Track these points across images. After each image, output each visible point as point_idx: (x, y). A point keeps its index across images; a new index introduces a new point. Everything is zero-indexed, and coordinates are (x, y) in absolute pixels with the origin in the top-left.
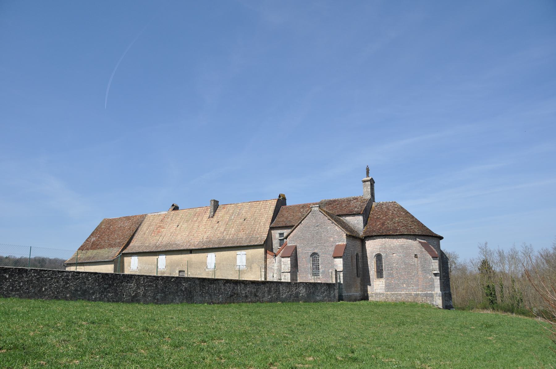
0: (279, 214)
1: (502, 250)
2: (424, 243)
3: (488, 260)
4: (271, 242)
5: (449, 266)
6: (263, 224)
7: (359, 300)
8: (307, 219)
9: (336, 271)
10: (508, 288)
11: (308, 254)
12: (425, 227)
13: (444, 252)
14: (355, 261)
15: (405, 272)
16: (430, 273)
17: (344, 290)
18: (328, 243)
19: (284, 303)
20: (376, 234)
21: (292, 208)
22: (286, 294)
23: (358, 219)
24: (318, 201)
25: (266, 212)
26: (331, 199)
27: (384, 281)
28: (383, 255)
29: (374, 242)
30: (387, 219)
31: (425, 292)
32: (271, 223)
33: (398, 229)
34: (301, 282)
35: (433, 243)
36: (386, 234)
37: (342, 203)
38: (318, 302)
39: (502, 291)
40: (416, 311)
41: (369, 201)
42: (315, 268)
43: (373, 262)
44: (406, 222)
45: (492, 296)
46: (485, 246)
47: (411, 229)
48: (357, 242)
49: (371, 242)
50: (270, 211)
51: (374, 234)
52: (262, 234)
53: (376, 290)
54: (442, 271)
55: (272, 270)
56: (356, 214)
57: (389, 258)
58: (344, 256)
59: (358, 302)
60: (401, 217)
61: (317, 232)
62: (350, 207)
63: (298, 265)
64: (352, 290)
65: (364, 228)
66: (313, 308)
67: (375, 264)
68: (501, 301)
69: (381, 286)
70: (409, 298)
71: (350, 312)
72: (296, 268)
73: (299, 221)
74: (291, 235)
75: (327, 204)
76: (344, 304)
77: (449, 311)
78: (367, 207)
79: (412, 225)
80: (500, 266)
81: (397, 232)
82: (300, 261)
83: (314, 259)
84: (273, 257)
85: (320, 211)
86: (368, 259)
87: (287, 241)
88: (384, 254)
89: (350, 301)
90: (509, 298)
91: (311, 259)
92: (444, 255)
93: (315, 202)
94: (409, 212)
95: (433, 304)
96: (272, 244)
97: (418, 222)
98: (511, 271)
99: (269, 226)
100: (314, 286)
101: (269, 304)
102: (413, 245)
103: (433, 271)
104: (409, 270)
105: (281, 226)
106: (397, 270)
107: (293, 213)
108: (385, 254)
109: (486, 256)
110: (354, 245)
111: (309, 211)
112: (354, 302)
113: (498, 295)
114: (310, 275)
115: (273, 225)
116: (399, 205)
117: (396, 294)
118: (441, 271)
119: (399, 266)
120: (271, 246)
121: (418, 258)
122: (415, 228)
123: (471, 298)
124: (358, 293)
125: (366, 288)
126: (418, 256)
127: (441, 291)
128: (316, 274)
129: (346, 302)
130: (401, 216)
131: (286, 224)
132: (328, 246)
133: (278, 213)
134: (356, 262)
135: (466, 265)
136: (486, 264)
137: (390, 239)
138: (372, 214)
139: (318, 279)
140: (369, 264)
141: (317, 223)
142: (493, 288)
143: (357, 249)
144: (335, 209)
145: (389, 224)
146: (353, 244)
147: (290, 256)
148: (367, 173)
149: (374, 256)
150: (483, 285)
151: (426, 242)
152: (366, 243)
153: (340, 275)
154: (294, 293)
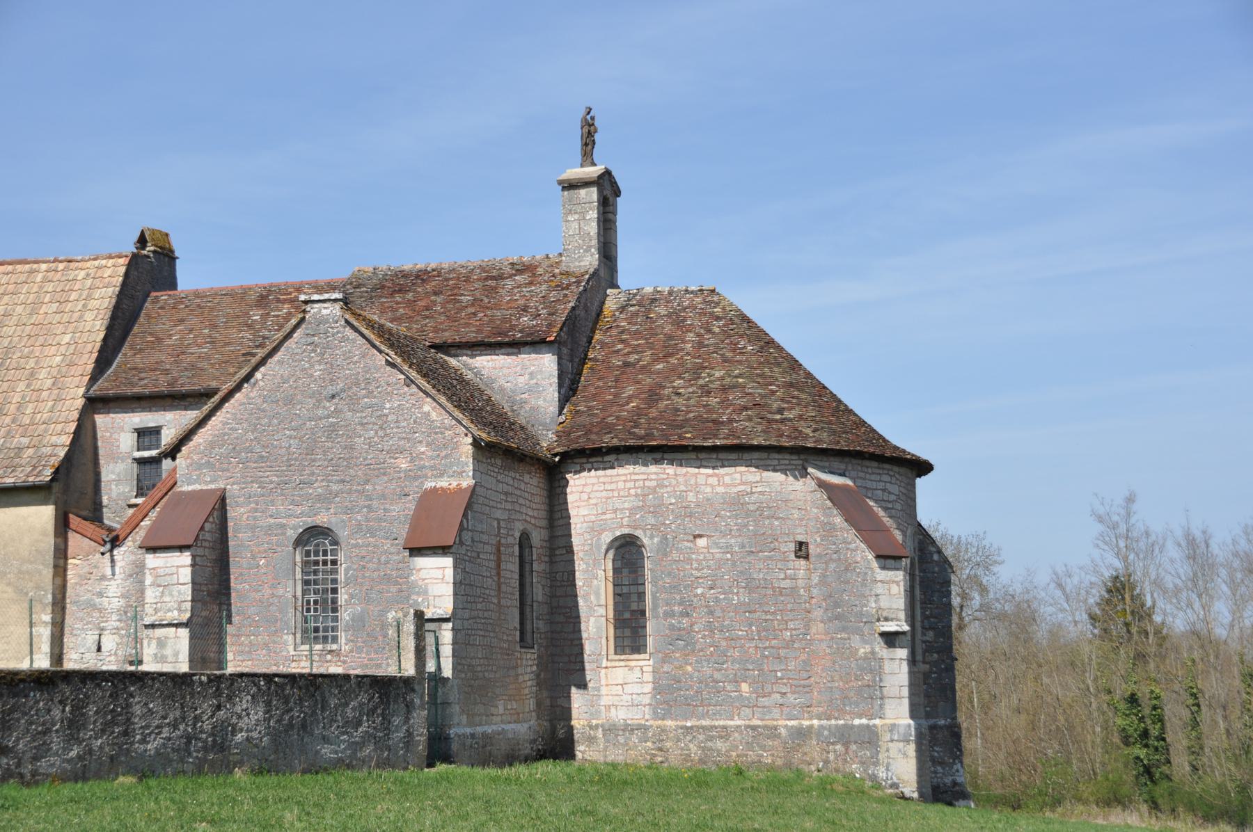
0: (136, 329)
1: (1204, 532)
2: (844, 488)
3: (1138, 575)
4: (91, 476)
5: (956, 601)
6: (49, 382)
7: (527, 760)
8: (281, 362)
9: (419, 615)
10: (1224, 708)
11: (284, 534)
12: (850, 412)
13: (936, 535)
14: (515, 567)
15: (751, 625)
16: (866, 630)
17: (456, 709)
18: (386, 478)
19: (152, 782)
20: (615, 442)
21: (202, 302)
22: (166, 732)
23: (533, 368)
24: (342, 273)
25: (66, 318)
27: (650, 669)
28: (646, 541)
30: (671, 372)
31: (842, 722)
32: (94, 378)
33: (725, 418)
34: (246, 670)
35: (884, 490)
37: (456, 287)
38: (326, 770)
39: (1195, 724)
40: (795, 810)
41: (588, 281)
42: (316, 602)
43: (601, 573)
44: (760, 385)
45: (1146, 746)
46: (1123, 512)
47: (783, 421)
48: (527, 478)
49: (594, 480)
50: (89, 316)
51: (608, 440)
52: (46, 431)
53: (608, 708)
54: (922, 622)
55: (96, 614)
56: (525, 344)
57: (675, 555)
58: (461, 543)
59: (521, 770)
60: (740, 362)
61: (332, 425)
62: (497, 307)
63: (228, 588)
64: (493, 710)
65: (560, 414)
66: (298, 803)
68: (1188, 768)
69: (637, 689)
70: (763, 748)
71: (483, 818)
72: (221, 604)
73: (240, 368)
74: (199, 439)
75: (383, 287)
76: (455, 777)
77: (948, 809)
79: (788, 402)
80: (1190, 605)
81: (716, 436)
83: (313, 558)
84: (102, 549)
85: (347, 322)
86: (577, 563)
87: (174, 470)
88: (652, 537)
89: (484, 763)
90: (1229, 754)
91: (298, 559)
92: (933, 549)
93: (323, 276)
95: (874, 778)
96: (97, 475)
97: (819, 391)
98: (1241, 629)
99: (81, 391)
100: (308, 690)
101: (67, 790)
102: (791, 497)
103: (878, 620)
104: (769, 617)
105: (147, 391)
106: (711, 613)
107: (214, 326)
108: (656, 540)
109: (1125, 559)
110: (511, 489)
111: (294, 321)
112: (501, 765)
113: (1178, 740)
114: (291, 637)
115: (104, 386)
116: (731, 304)
117: (703, 728)
118: (918, 625)
120: (90, 490)
121: (812, 559)
123: (1050, 752)
124: (526, 726)
125: (559, 702)
126: (812, 549)
127: (912, 717)
128: (321, 634)
129: (465, 769)
130: (738, 358)
131: (175, 379)
132: (383, 497)
133: (131, 329)
134: (517, 576)
135: (1035, 598)
136: (1127, 597)
137: (681, 466)
138: (603, 345)
139: (329, 657)
140: (579, 583)
141: (332, 380)
142: (1155, 708)
143: (524, 510)
144: (427, 313)
145: (678, 394)
146: (506, 488)
147: (190, 542)
148: (586, 144)
149: (604, 547)
150: (1109, 692)
151: (849, 482)
152: (568, 482)
153: (437, 638)
154: (207, 726)
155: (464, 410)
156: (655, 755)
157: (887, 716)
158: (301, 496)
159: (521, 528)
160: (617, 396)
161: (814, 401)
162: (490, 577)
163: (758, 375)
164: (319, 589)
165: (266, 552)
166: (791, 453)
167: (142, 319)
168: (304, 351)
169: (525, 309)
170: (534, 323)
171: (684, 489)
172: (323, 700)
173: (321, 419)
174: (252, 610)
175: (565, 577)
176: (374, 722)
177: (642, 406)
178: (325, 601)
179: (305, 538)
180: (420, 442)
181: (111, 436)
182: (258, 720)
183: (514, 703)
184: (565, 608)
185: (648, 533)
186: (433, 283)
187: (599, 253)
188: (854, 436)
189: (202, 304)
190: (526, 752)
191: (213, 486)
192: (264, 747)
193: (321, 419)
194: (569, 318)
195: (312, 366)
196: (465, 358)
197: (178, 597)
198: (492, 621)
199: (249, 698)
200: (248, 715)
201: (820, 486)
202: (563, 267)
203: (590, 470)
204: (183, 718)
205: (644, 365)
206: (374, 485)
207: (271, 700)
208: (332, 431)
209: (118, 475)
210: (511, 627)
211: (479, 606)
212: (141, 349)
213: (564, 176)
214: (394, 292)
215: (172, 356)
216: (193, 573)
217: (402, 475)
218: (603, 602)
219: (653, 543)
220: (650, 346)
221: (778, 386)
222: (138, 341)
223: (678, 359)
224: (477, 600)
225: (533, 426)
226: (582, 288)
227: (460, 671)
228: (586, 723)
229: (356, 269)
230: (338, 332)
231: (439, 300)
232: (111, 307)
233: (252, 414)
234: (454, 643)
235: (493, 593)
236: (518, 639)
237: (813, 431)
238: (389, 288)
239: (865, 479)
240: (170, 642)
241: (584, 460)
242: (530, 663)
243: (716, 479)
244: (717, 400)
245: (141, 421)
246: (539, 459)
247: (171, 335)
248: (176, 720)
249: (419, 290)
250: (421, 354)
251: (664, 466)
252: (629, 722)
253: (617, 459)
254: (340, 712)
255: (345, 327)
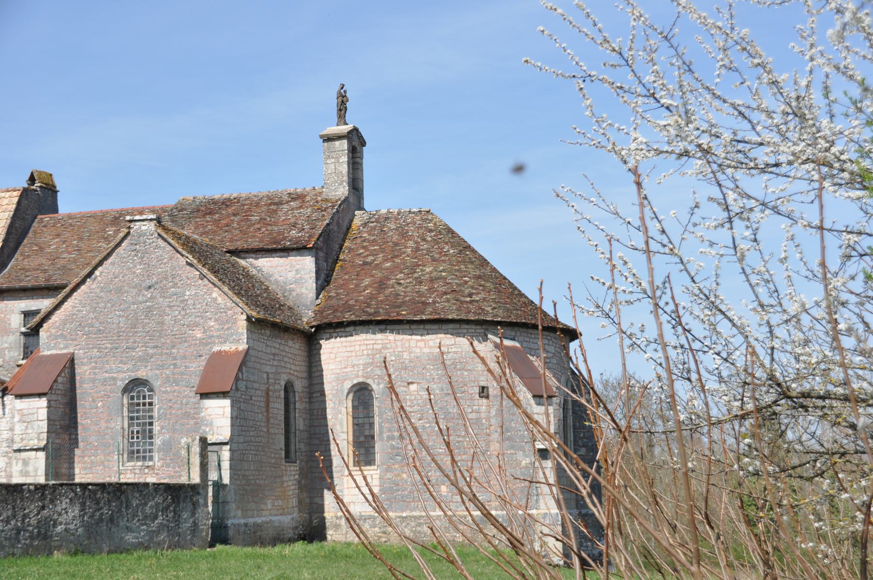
0: (25, 241)
2: (513, 349)
8: (113, 264)
9: (203, 441)
11: (115, 384)
12: (521, 295)
17: (233, 506)
18: (186, 344)
20: (353, 318)
23: (298, 266)
26: (217, 197)
27: (378, 476)
28: (374, 387)
29: (349, 344)
30: (396, 268)
33: (431, 300)
36: (386, 318)
37: (249, 210)
41: (340, 205)
42: (138, 432)
43: (344, 410)
47: (471, 302)
48: (290, 343)
49: (339, 345)
51: (349, 317)
56: (293, 249)
58: (237, 389)
59: (287, 550)
60: (444, 261)
61: (149, 307)
62: (276, 224)
63: (76, 423)
64: (263, 507)
65: (317, 298)
67: (350, 419)
72: (70, 434)
74: (55, 318)
78: (334, 227)
79: (477, 289)
81: (423, 313)
82: (85, 408)
83: (136, 401)
85: (159, 235)
86: (327, 403)
88: (379, 384)
91: (125, 401)
94: (472, 245)
104: (460, 439)
105: (30, 285)
107: (81, 239)
108: (381, 386)
110: (277, 351)
111: (122, 235)
116: (441, 221)
117: (415, 517)
119: (428, 425)
121: (491, 398)
122: (484, 299)
124: (289, 517)
125: (316, 500)
128: (141, 454)
131: (50, 276)
132: (184, 357)
134: (282, 412)
137: (399, 334)
138: (350, 250)
139: (146, 471)
140: (329, 417)
141: (148, 276)
143: (288, 366)
144: (227, 228)
145: (400, 284)
146: (274, 351)
148: (340, 110)
151: (517, 345)
152: (321, 346)
153: (219, 457)
154: (34, 521)
155: (242, 296)
156: (381, 537)
157: (541, 507)
158: (127, 357)
159: (286, 378)
160: (357, 285)
161: (495, 288)
162: (261, 413)
163: (458, 270)
164: (140, 423)
165: (102, 397)
166: (476, 325)
167: (30, 235)
168: (130, 255)
169: (294, 225)
170: (300, 235)
171: (401, 350)
172: (127, 502)
173: (141, 303)
174: (92, 439)
175: (320, 413)
176: (167, 516)
177: (374, 292)
178: (144, 431)
179: (130, 387)
180: (210, 319)
181: (5, 317)
182: (74, 516)
183: (280, 501)
184: (320, 434)
185: (376, 381)
186: (234, 208)
187: (349, 186)
188: (522, 313)
189: (73, 224)
190: (290, 536)
191: (65, 351)
192: (79, 536)
193: (141, 303)
194: (324, 231)
195: (135, 266)
196: (251, 260)
197: (38, 429)
198: (262, 444)
199: (68, 500)
200: (67, 512)
201: (496, 347)
202: (324, 196)
203: (336, 338)
204: (14, 516)
205: (377, 264)
206: (178, 349)
207: (85, 501)
208: (149, 312)
209: (10, 344)
210: (278, 448)
211: (252, 434)
212: (28, 255)
213: (325, 132)
214: (206, 214)
215: (50, 260)
216: (48, 413)
217: (198, 342)
218: (345, 430)
219: (379, 389)
220: (382, 250)
221: (470, 278)
222: (27, 249)
223: (401, 259)
224: (250, 429)
225: (298, 307)
226: (335, 210)
227: (236, 479)
228: (333, 515)
229: (181, 198)
230: (153, 242)
231: (236, 219)
232: (7, 226)
233: (93, 300)
234: (231, 459)
235: (263, 424)
236: (283, 456)
237: (493, 309)
238: (202, 211)
239: (529, 342)
240: (32, 462)
241: (332, 331)
242: (293, 473)
243: (423, 343)
244: (426, 288)
245: (26, 306)
246: (299, 330)
247: (50, 245)
248: (8, 517)
249: (223, 212)
250: (217, 257)
251: (387, 334)
252: (363, 514)
253: (355, 330)
254: (140, 509)
255: (158, 239)
